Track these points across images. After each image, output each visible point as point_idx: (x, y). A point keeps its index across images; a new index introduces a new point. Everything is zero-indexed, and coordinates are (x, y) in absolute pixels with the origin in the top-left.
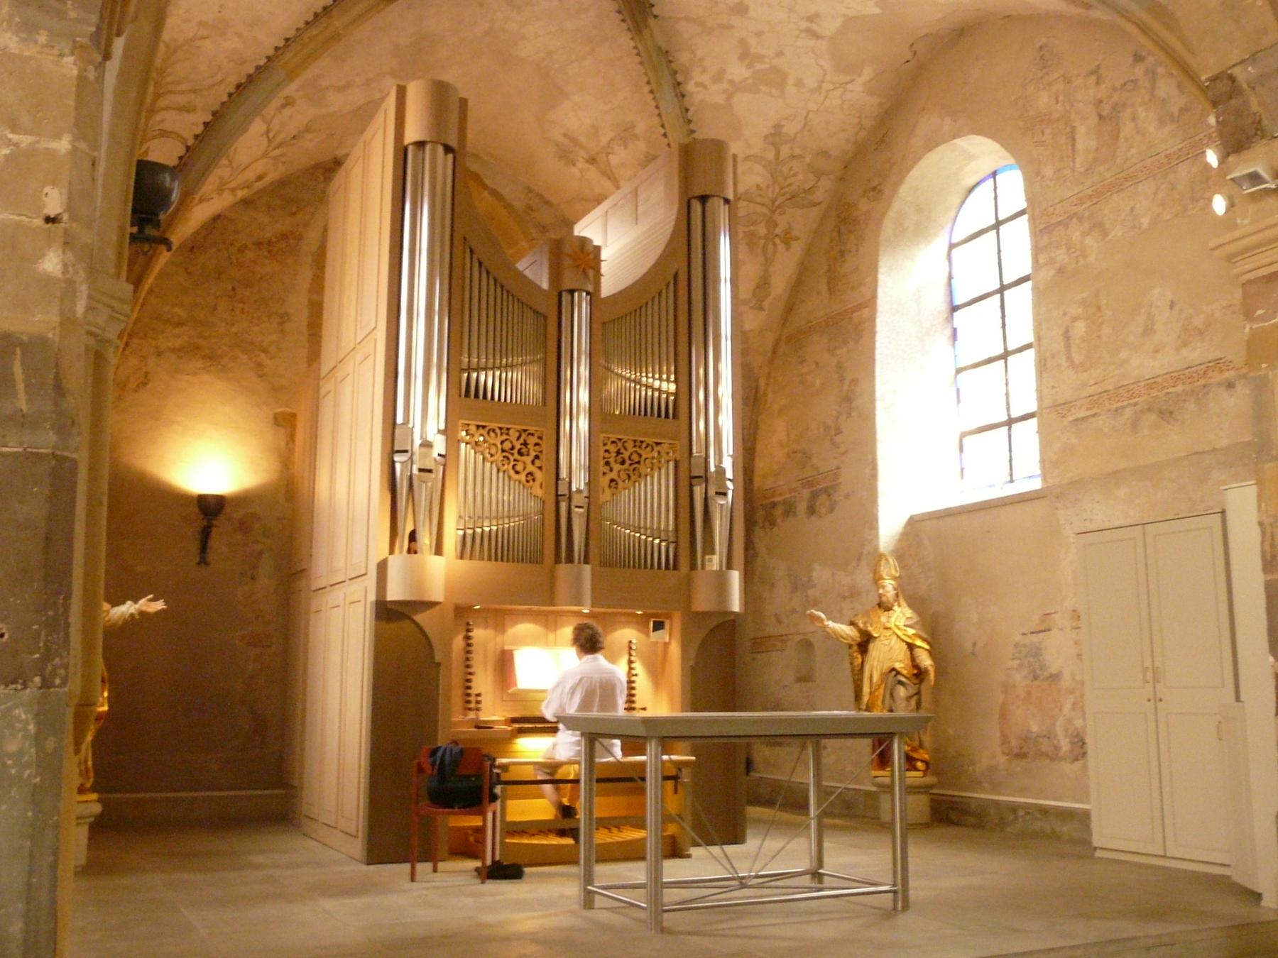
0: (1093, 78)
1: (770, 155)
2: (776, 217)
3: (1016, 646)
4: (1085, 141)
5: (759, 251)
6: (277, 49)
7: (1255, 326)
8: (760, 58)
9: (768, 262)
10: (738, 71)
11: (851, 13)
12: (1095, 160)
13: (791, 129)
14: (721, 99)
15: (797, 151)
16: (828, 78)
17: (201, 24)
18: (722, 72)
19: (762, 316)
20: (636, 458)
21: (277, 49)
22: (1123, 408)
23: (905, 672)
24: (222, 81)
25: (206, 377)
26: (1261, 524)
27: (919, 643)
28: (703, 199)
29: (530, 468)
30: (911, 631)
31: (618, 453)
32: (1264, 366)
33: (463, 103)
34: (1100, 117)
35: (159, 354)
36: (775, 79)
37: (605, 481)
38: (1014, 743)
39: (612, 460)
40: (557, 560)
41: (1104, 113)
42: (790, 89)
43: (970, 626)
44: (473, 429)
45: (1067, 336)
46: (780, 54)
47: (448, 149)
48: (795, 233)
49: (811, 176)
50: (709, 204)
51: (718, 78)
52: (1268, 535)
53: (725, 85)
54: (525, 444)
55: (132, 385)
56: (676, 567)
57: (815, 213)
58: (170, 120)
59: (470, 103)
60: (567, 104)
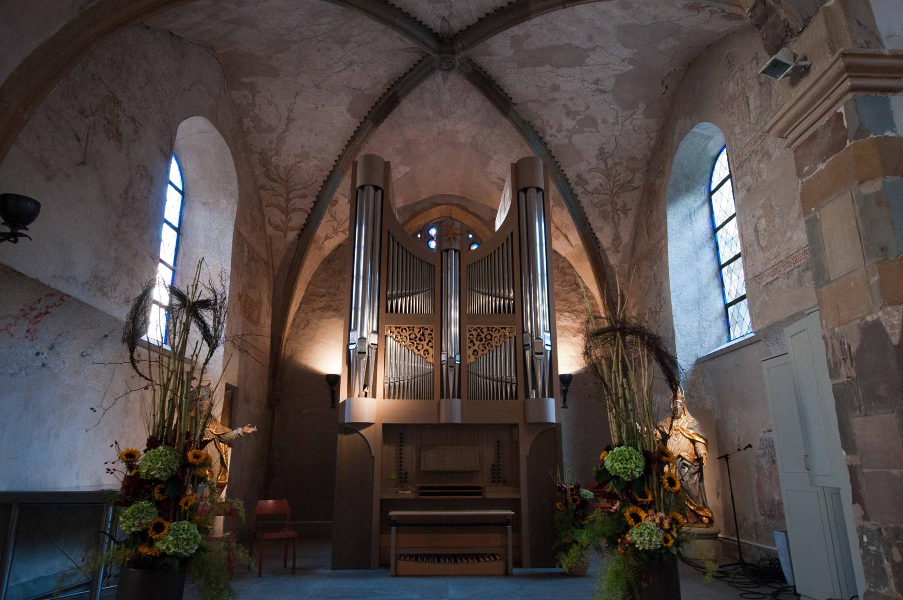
0: (755, 62)
1: (602, 166)
2: (615, 199)
3: (761, 440)
4: (754, 102)
5: (610, 220)
6: (336, 161)
7: (804, 180)
8: (577, 113)
9: (616, 226)
10: (569, 123)
11: (618, 73)
12: (760, 113)
13: (609, 148)
14: (566, 141)
15: (617, 161)
16: (619, 115)
17: (296, 156)
18: (560, 125)
19: (620, 255)
20: (489, 337)
21: (336, 161)
22: (792, 270)
23: (688, 458)
24: (316, 181)
25: (334, 319)
26: (824, 337)
27: (697, 438)
28: (525, 190)
29: (426, 347)
30: (691, 432)
31: (478, 335)
32: (813, 209)
33: (387, 164)
34: (760, 84)
35: (314, 311)
36: (590, 122)
37: (470, 352)
38: (767, 507)
39: (474, 340)
40: (442, 397)
41: (762, 81)
42: (601, 126)
43: (744, 426)
44: (393, 329)
45: (756, 231)
46: (588, 108)
47: (376, 188)
48: (628, 207)
49: (629, 173)
50: (529, 191)
51: (560, 130)
52: (830, 345)
53: (565, 133)
54: (423, 335)
55: (302, 326)
56: (516, 398)
57: (637, 193)
58: (297, 203)
59: (392, 165)
60: (492, 162)
